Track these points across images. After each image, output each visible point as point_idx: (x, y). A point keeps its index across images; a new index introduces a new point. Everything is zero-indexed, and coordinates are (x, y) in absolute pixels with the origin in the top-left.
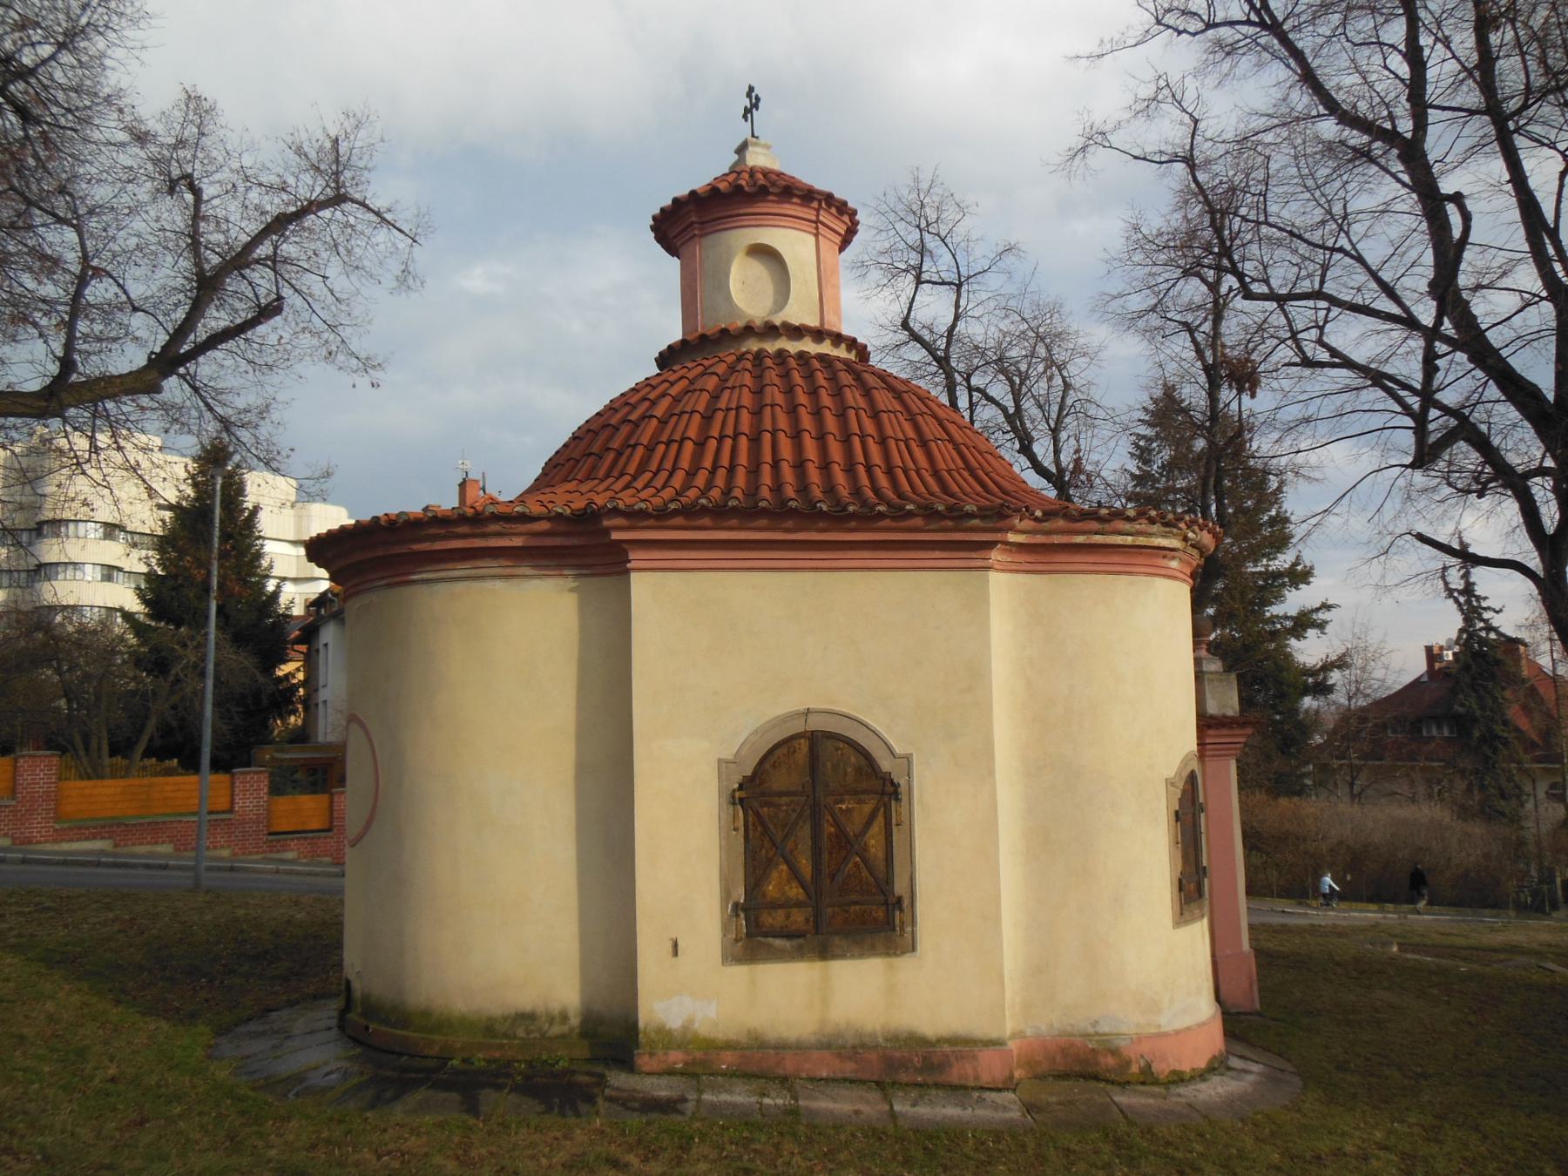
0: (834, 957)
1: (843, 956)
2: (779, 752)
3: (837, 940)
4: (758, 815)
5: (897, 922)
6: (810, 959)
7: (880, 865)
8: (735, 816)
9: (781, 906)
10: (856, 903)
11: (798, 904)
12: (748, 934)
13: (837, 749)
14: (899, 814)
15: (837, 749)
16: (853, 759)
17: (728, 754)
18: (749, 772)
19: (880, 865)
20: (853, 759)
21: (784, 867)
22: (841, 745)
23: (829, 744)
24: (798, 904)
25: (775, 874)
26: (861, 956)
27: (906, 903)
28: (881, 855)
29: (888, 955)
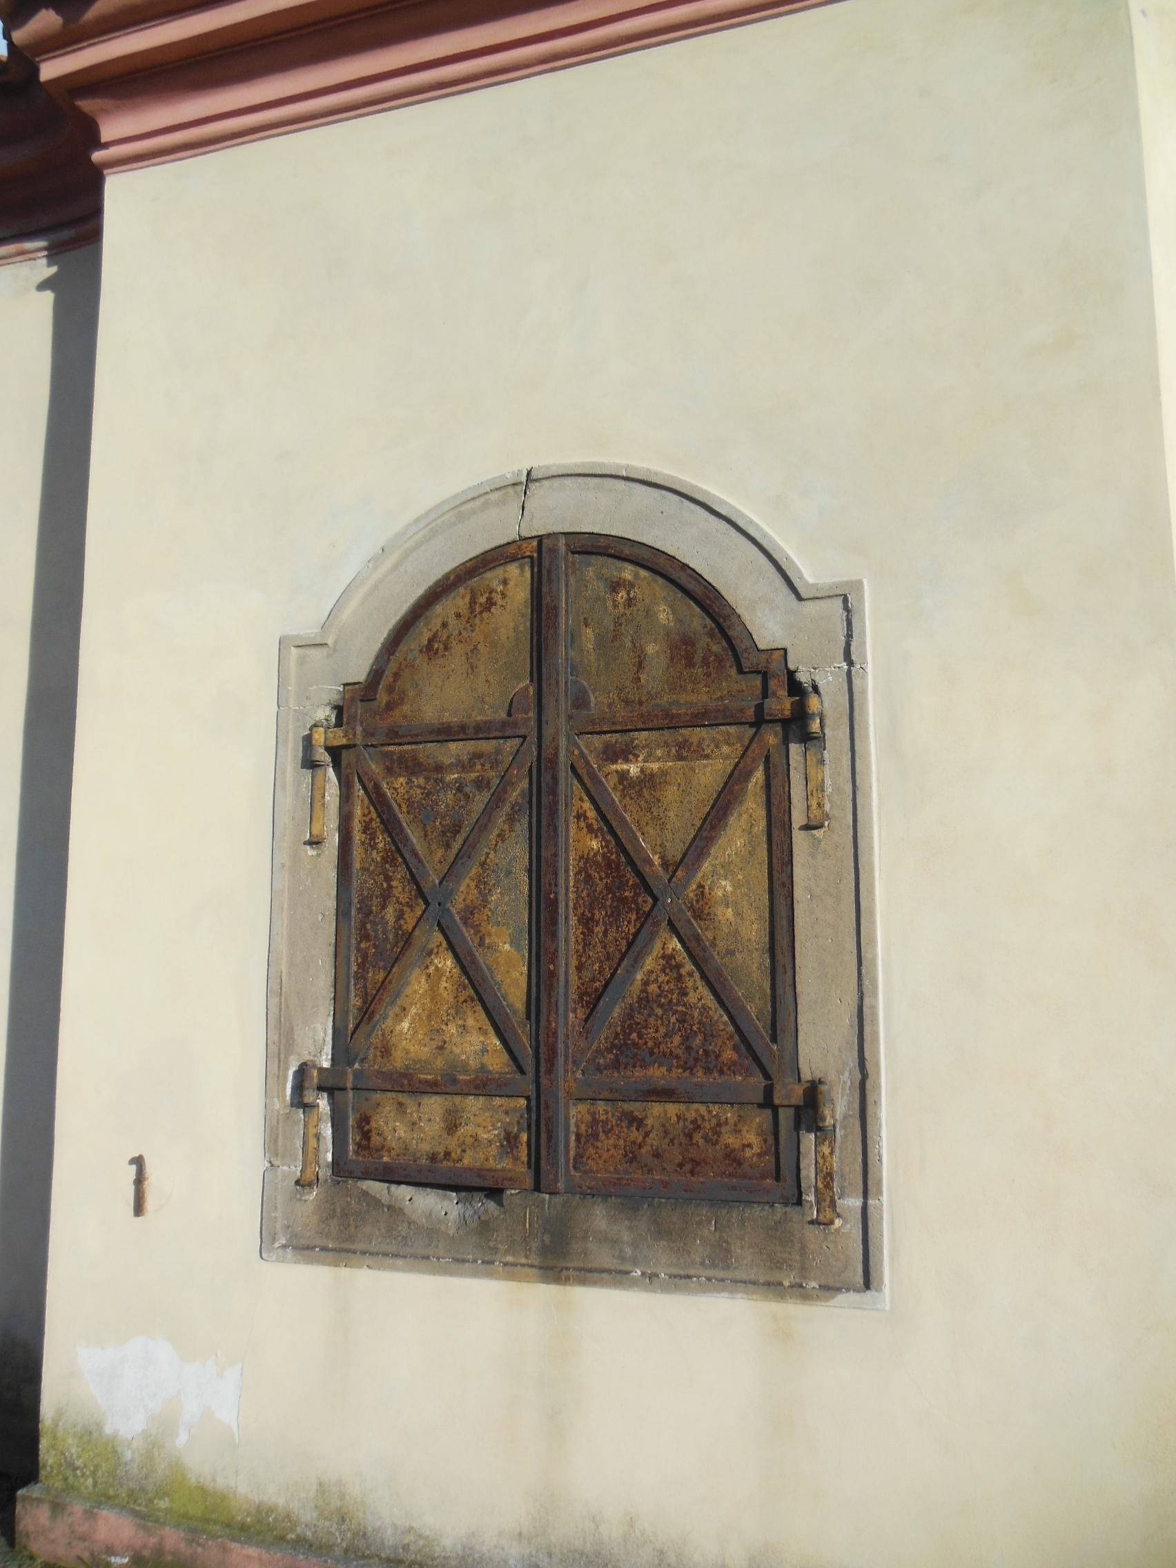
0: (588, 1275)
1: (617, 1276)
2: (443, 610)
3: (599, 1217)
4: (377, 799)
5: (809, 1172)
6: (511, 1272)
7: (755, 1008)
8: (315, 802)
9: (433, 1088)
10: (666, 1094)
11: (483, 1085)
12: (340, 1168)
13: (615, 586)
14: (815, 790)
15: (615, 586)
16: (664, 615)
17: (306, 623)
18: (359, 671)
19: (755, 1008)
20: (664, 615)
21: (447, 963)
22: (628, 572)
23: (594, 570)
24: (483, 1085)
25: (417, 985)
26: (681, 1281)
27: (838, 1108)
28: (754, 930)
29: (774, 1289)
